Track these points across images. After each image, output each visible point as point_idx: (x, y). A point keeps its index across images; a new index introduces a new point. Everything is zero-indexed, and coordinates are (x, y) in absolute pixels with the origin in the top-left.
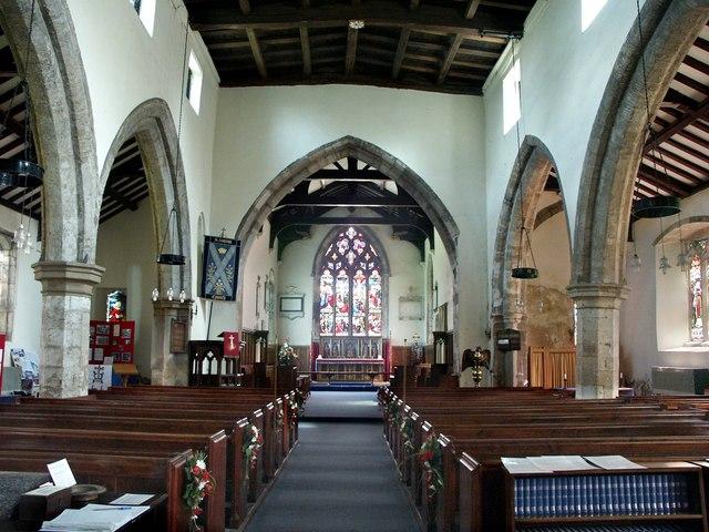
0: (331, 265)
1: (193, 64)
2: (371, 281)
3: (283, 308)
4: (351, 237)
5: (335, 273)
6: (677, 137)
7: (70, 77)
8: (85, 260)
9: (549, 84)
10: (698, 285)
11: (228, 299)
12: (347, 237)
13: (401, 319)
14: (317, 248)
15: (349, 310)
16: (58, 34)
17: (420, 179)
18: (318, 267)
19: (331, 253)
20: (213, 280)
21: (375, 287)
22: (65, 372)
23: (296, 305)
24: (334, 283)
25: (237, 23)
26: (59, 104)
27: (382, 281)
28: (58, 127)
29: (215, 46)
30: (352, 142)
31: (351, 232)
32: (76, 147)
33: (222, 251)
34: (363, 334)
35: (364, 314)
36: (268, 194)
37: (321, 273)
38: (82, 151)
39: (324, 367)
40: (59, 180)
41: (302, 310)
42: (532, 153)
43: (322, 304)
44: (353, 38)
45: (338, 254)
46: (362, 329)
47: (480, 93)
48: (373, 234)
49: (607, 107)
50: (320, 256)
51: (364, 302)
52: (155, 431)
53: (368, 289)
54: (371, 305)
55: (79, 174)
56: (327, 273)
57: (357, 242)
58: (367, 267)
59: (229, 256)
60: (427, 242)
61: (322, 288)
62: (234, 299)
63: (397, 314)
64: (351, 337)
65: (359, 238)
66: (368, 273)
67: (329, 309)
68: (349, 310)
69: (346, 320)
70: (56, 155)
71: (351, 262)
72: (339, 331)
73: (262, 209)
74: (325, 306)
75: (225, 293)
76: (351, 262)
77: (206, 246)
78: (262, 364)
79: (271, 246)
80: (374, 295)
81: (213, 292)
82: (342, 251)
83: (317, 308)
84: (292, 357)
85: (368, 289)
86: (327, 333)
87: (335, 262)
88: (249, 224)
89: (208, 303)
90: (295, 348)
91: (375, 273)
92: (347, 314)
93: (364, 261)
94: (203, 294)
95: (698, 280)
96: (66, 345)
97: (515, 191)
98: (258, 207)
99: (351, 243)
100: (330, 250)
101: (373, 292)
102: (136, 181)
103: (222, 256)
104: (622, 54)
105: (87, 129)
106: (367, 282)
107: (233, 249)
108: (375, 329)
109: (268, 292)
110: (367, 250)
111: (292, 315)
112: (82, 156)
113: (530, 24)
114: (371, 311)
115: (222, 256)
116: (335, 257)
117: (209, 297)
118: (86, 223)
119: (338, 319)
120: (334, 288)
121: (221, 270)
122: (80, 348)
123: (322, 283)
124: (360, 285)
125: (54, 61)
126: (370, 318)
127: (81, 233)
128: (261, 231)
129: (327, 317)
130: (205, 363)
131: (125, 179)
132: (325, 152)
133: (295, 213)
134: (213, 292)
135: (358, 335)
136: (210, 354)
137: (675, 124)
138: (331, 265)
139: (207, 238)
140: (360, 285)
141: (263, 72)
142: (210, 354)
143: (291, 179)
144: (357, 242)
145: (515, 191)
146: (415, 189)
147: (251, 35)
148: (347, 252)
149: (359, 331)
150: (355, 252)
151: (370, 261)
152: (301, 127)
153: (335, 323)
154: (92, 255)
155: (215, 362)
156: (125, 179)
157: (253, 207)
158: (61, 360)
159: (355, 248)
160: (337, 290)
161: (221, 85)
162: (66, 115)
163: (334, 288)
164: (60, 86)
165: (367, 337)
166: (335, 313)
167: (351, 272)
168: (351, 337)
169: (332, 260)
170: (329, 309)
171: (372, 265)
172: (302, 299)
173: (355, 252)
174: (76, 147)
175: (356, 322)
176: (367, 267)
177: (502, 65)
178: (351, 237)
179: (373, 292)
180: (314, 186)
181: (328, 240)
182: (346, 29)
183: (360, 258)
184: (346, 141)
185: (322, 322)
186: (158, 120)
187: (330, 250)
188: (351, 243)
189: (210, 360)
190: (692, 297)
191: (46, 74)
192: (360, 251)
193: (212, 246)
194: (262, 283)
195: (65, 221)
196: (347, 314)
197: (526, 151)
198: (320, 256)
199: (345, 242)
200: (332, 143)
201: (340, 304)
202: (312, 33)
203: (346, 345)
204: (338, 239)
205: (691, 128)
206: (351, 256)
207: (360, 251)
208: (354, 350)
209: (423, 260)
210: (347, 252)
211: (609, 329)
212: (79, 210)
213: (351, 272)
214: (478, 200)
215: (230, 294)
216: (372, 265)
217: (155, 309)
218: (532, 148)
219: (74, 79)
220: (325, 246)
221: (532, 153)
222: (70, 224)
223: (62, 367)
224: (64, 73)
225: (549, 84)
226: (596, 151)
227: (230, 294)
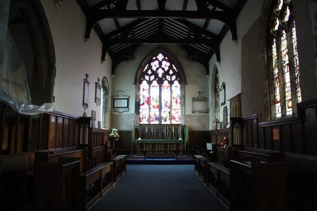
3: (115, 106)
4: (160, 60)
5: (150, 82)
15: (160, 107)
19: (147, 70)
23: (124, 103)
24: (149, 88)
37: (141, 82)
45: (152, 70)
46: (168, 119)
56: (144, 83)
58: (171, 79)
66: (171, 83)
72: (153, 121)
74: (143, 104)
82: (154, 68)
91: (176, 83)
93: (169, 75)
99: (160, 63)
100: (146, 68)
110: (171, 67)
116: (150, 72)
120: (149, 92)
148: (157, 69)
150: (163, 69)
167: (160, 82)
172: (128, 100)
173: (163, 69)
175: (164, 115)
176: (171, 79)
181: (145, 61)
183: (166, 73)
187: (146, 68)
188: (160, 63)
192: (166, 69)
210: (157, 69)
213: (160, 82)
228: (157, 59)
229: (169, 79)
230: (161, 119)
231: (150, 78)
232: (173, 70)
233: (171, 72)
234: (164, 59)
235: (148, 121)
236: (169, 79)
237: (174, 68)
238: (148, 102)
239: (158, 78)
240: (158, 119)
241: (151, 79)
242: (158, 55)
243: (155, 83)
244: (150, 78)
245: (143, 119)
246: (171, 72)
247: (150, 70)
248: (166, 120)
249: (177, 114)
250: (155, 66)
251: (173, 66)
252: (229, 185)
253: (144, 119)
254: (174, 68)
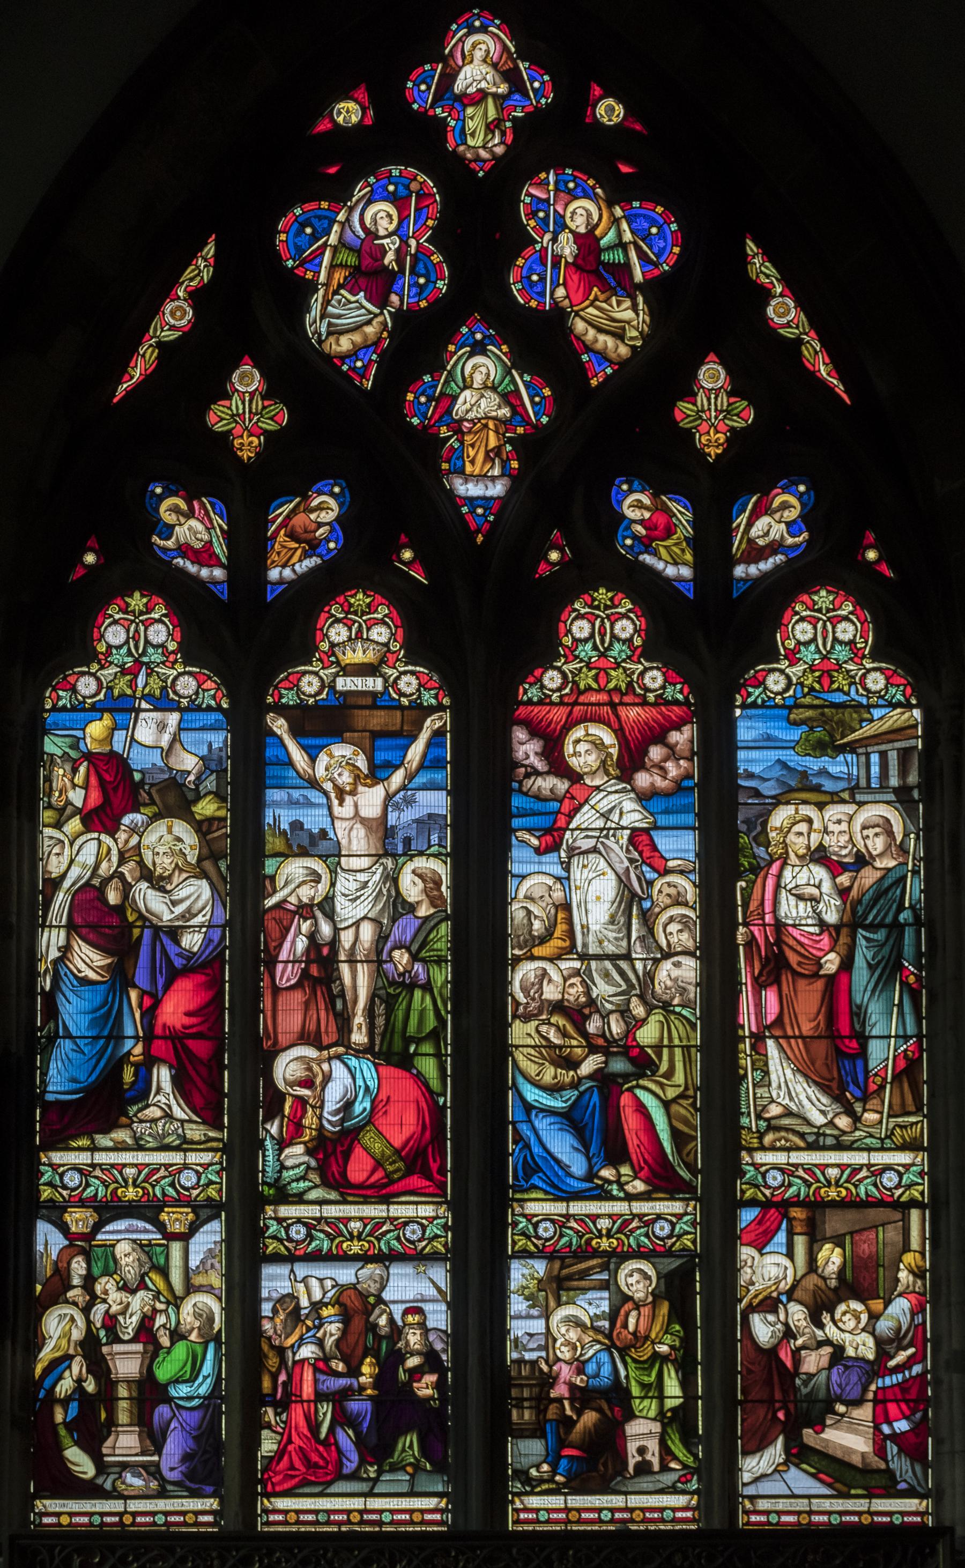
0: (190, 528)
2: (762, 747)
4: (479, 138)
5: (249, 639)
15: (468, 1157)
19: (196, 371)
24: (248, 772)
43: (61, 1076)
45: (301, 374)
46: (642, 1434)
54: (785, 1086)
56: (135, 631)
58: (712, 547)
66: (713, 637)
68: (468, 1157)
69: (416, 1293)
71: (480, 484)
72: (321, 1472)
74: (106, 1104)
76: (480, 484)
78: (169, 1400)
82: (346, 324)
87: (248, 493)
91: (825, 632)
93: (669, 462)
99: (479, 223)
100: (175, 317)
106: (717, 749)
110: (700, 309)
114: (770, 1165)
116: (245, 409)
120: (239, 858)
123: (72, 789)
126: (766, 1267)
138: (190, 528)
141: (490, 101)
148: (418, 345)
149: (599, 1462)
150: (541, 343)
159: (540, 281)
160: (292, 878)
163: (239, 858)
166: (245, 1206)
167: (483, 625)
169: (206, 468)
171: (773, 524)
173: (541, 343)
175: (552, 1331)
176: (712, 547)
178: (479, 138)
179: (802, 899)
183: (599, 433)
185: (59, 1327)
187: (175, 317)
188: (479, 223)
192: (612, 328)
196: (421, 1214)
207: (612, 328)
210: (418, 345)
211: (188, 762)
213: (483, 625)
216: (773, 524)
228: (409, 137)
229: (674, 565)
230: (500, 1429)
231: (248, 547)
232: (764, 367)
233: (713, 409)
234: (550, 140)
235: (201, 1473)
236: (674, 565)
237: (783, 313)
238: (225, 1070)
239: (437, 519)
240: (431, 1423)
241: (286, 568)
242: (33, 1506)
243: (360, 645)
244: (248, 547)
245: (93, 1435)
246: (713, 409)
247: (247, 380)
248: (599, 1462)
249: (851, 1331)
250: (370, 276)
251: (761, 269)
252: (751, 943)
253: (125, 1443)
254: (783, 313)
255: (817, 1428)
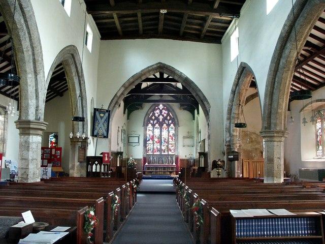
0: (152, 122)
1: (89, 29)
2: (170, 129)
3: (130, 141)
4: (161, 109)
5: (153, 125)
6: (310, 63)
7: (32, 36)
8: (39, 119)
9: (252, 38)
10: (320, 131)
11: (105, 137)
12: (159, 109)
13: (184, 146)
14: (145, 114)
15: (160, 142)
16: (27, 16)
17: (192, 82)
18: (146, 122)
19: (152, 116)
20: (98, 129)
21: (172, 132)
22: (30, 170)
23: (136, 140)
24: (153, 130)
25: (109, 10)
26: (27, 48)
27: (175, 129)
28: (27, 58)
29: (98, 21)
30: (161, 65)
31: (161, 106)
32: (35, 67)
33: (102, 115)
34: (166, 153)
35: (167, 144)
36: (123, 89)
37: (147, 125)
38: (38, 69)
39: (148, 168)
40: (27, 83)
41: (139, 142)
42: (244, 70)
43: (148, 139)
44: (162, 18)
45: (155, 117)
46: (166, 151)
47: (220, 43)
48: (171, 107)
49: (278, 49)
50: (147, 117)
51: (167, 138)
52: (71, 198)
53: (169, 133)
54: (170, 140)
55: (36, 80)
56: (150, 125)
57: (164, 111)
58: (168, 123)
59: (105, 118)
60: (196, 111)
61: (148, 132)
62: (107, 137)
63: (182, 144)
64: (161, 155)
65: (165, 109)
66: (168, 125)
67: (151, 142)
68: (160, 142)
69: (159, 147)
70: (26, 71)
71: (161, 120)
72: (155, 152)
73: (120, 96)
74: (149, 140)
75: (103, 134)
76: (161, 120)
77: (95, 113)
79: (124, 113)
80: (171, 135)
81: (98, 134)
82: (157, 115)
83: (145, 141)
84: (134, 164)
85: (169, 133)
86: (150, 153)
87: (153, 120)
88: (114, 103)
89: (95, 139)
90: (135, 160)
91: (172, 125)
92: (159, 144)
93: (167, 120)
94: (93, 135)
95: (320, 128)
96: (30, 158)
97: (236, 88)
98: (118, 95)
99: (161, 111)
100: (151, 115)
101: (171, 134)
102: (62, 83)
103: (102, 118)
104: (285, 25)
105: (40, 59)
106: (168, 129)
107: (107, 114)
108: (172, 151)
109: (123, 134)
110: (168, 114)
111: (134, 144)
112: (38, 72)
113: (243, 11)
114: (170, 143)
115: (102, 118)
116: (153, 118)
117: (96, 136)
118: (40, 102)
119: (155, 147)
120: (153, 132)
121: (101, 124)
122: (37, 160)
123: (148, 130)
124: (165, 131)
125: (25, 28)
126: (170, 146)
127: (37, 107)
128: (120, 106)
129: (150, 145)
130: (94, 166)
131: (57, 82)
132: (149, 70)
133: (135, 98)
134: (98, 134)
135: (164, 154)
136: (96, 163)
137: (309, 57)
138: (152, 122)
139: (95, 109)
140: (165, 131)
142: (96, 163)
143: (133, 82)
144: (164, 111)
145: (236, 88)
146: (190, 87)
147: (115, 16)
148: (159, 116)
149: (164, 152)
150: (163, 116)
151: (170, 120)
152: (138, 58)
153: (153, 148)
154: (42, 117)
155: (98, 166)
156: (57, 82)
157: (116, 95)
158: (28, 165)
159: (163, 114)
160: (155, 133)
161: (101, 39)
162: (30, 53)
163: (153, 132)
164: (28, 39)
165: (168, 155)
166: (154, 143)
167: (161, 125)
168: (161, 155)
169: (152, 119)
170: (151, 142)
171: (170, 122)
172: (139, 137)
173: (163, 116)
174: (35, 67)
175: (163, 148)
176: (168, 123)
177: (230, 30)
178: (161, 109)
179: (171, 134)
180: (144, 85)
181: (151, 110)
182: (159, 13)
183: (165, 118)
184: (159, 65)
185: (148, 147)
186: (72, 55)
187: (151, 115)
188: (161, 111)
189: (96, 165)
190: (317, 136)
191: (21, 34)
192: (165, 115)
193: (97, 113)
194: (120, 130)
195: (30, 102)
196: (159, 144)
197: (241, 69)
198: (147, 117)
199: (158, 111)
200: (152, 66)
201: (156, 140)
202: (143, 15)
203: (159, 158)
204: (155, 110)
205: (317, 59)
206: (161, 117)
207: (165, 115)
208: (162, 161)
209: (194, 119)
210: (159, 116)
211: (279, 151)
212: (36, 96)
213: (161, 125)
214: (219, 92)
215: (105, 135)
216: (170, 122)
217: (71, 142)
218: (244, 68)
219: (34, 36)
220: (149, 113)
221: (244, 70)
222: (32, 103)
223: (28, 168)
224: (29, 33)
225: (252, 38)
226: (273, 69)
227: (105, 135)
255: (115, 17)
